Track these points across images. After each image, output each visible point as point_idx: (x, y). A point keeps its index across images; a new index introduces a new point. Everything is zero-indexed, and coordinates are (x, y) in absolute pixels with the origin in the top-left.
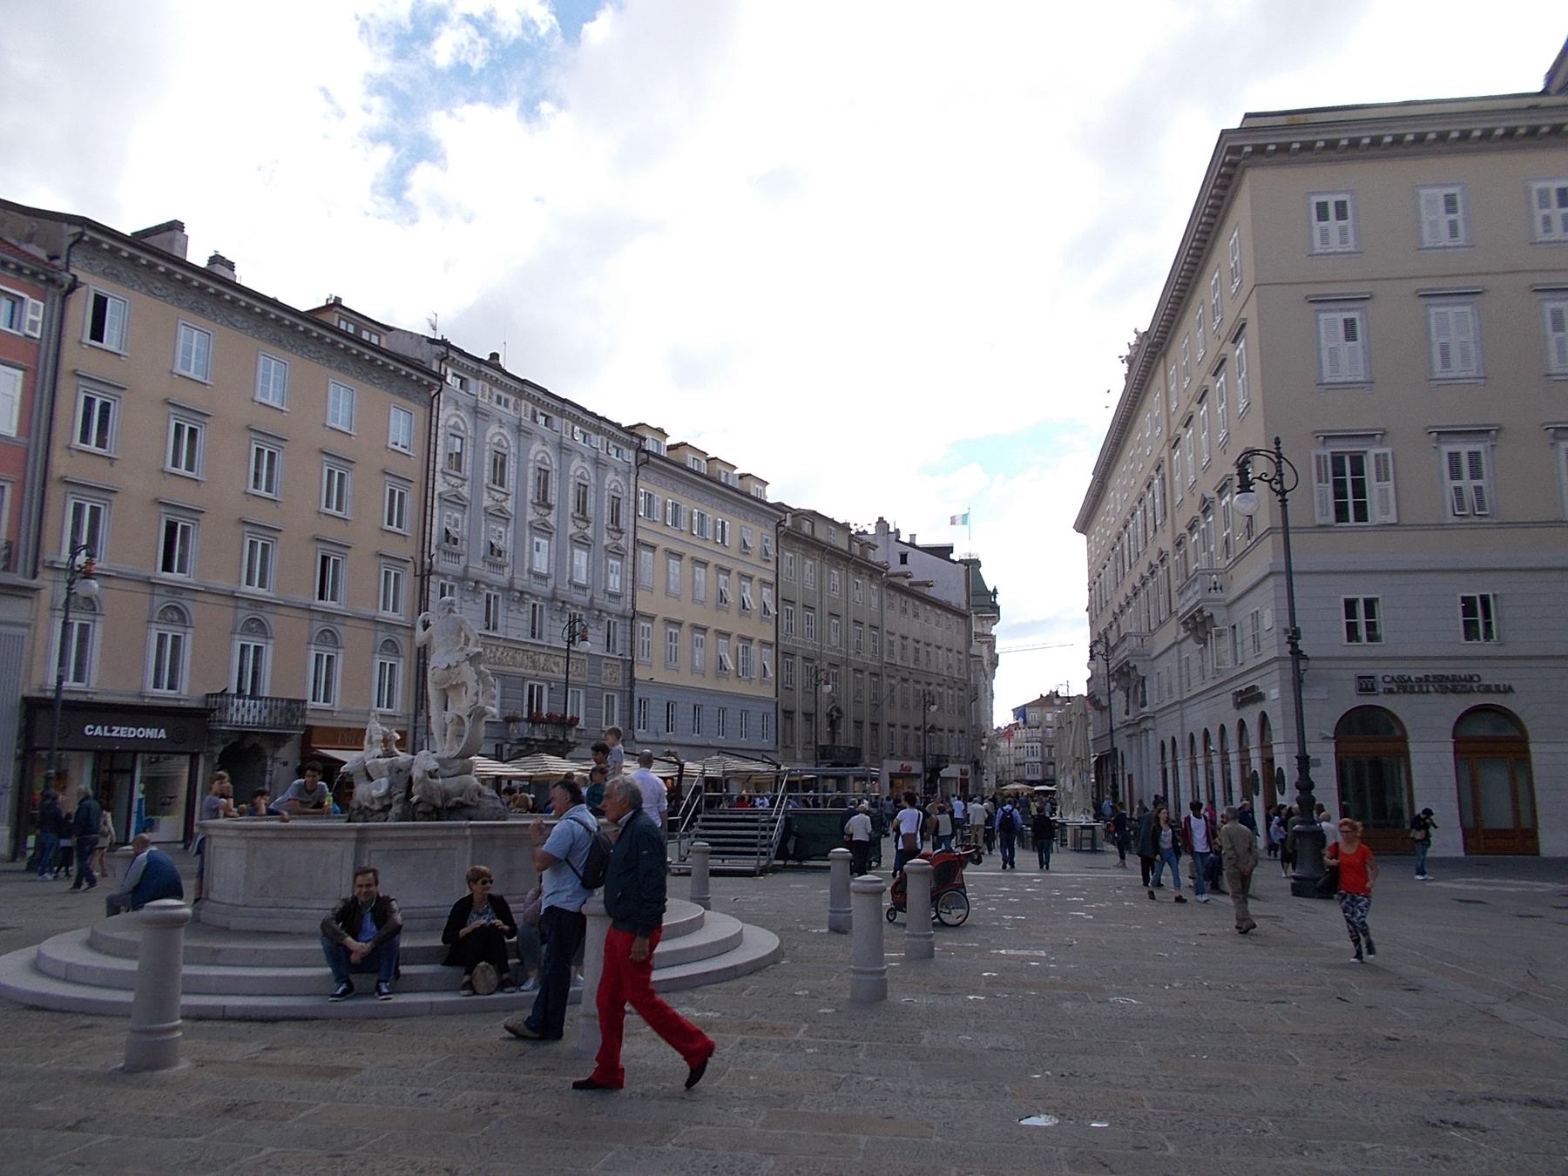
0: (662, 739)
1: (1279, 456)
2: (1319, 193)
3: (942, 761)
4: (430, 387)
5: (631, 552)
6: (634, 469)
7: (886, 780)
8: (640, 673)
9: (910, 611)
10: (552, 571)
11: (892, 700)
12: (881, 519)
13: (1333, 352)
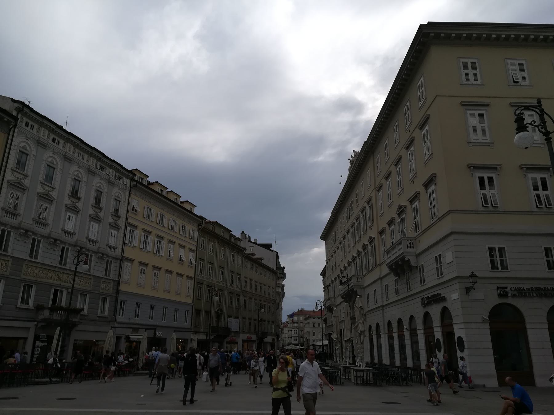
0: (132, 321)
1: (542, 111)
2: (464, 58)
3: (265, 334)
4: (8, 123)
5: (123, 227)
6: (129, 189)
7: (240, 343)
8: (122, 288)
9: (254, 269)
10: (77, 232)
11: (245, 307)
12: (243, 232)
13: (475, 129)
